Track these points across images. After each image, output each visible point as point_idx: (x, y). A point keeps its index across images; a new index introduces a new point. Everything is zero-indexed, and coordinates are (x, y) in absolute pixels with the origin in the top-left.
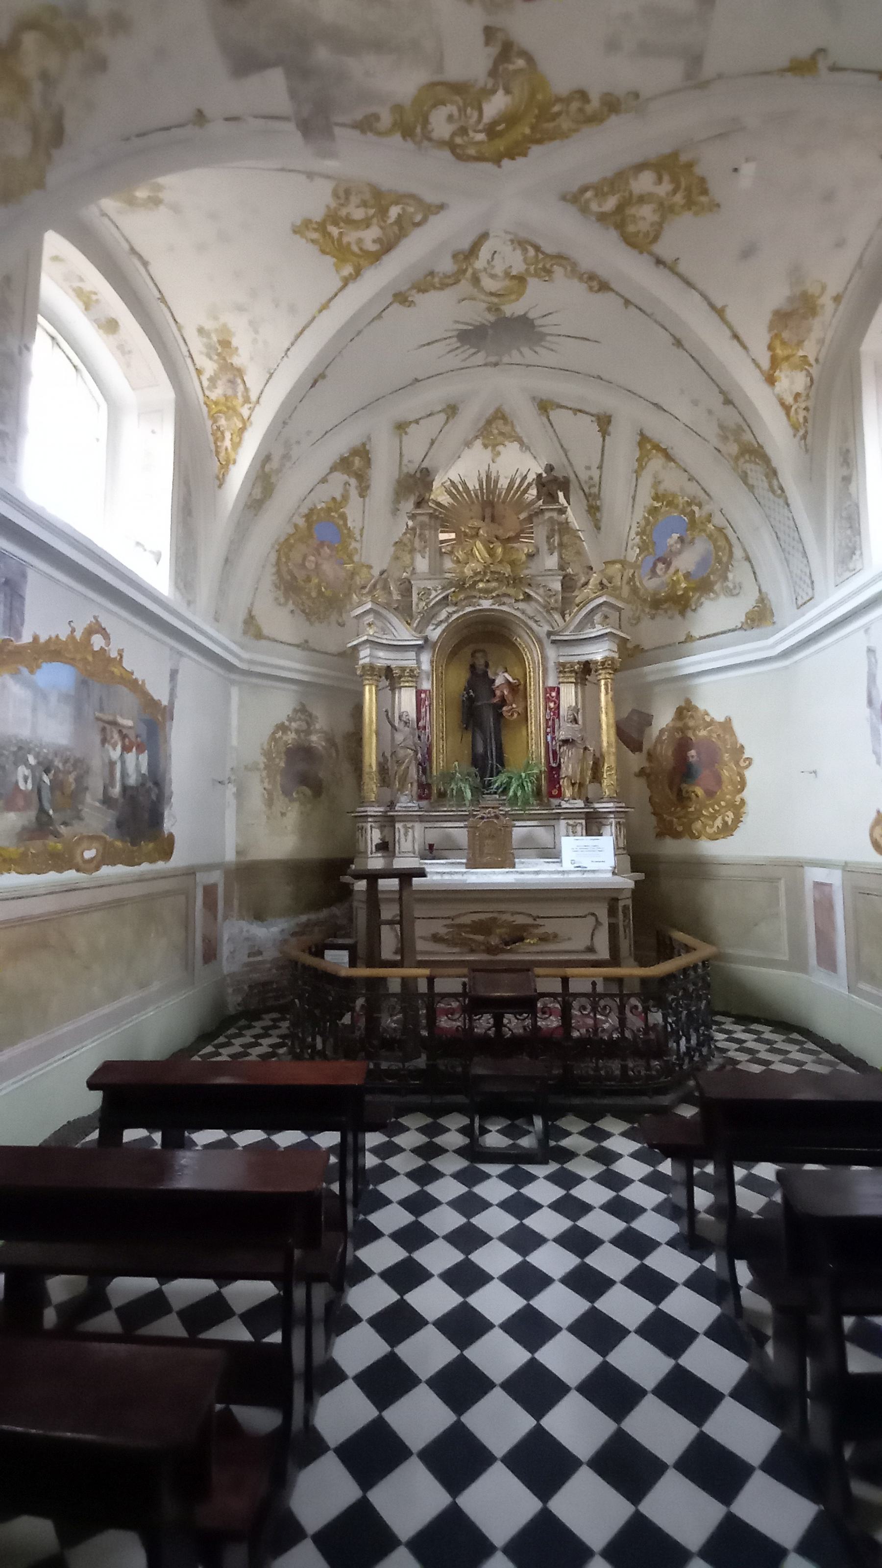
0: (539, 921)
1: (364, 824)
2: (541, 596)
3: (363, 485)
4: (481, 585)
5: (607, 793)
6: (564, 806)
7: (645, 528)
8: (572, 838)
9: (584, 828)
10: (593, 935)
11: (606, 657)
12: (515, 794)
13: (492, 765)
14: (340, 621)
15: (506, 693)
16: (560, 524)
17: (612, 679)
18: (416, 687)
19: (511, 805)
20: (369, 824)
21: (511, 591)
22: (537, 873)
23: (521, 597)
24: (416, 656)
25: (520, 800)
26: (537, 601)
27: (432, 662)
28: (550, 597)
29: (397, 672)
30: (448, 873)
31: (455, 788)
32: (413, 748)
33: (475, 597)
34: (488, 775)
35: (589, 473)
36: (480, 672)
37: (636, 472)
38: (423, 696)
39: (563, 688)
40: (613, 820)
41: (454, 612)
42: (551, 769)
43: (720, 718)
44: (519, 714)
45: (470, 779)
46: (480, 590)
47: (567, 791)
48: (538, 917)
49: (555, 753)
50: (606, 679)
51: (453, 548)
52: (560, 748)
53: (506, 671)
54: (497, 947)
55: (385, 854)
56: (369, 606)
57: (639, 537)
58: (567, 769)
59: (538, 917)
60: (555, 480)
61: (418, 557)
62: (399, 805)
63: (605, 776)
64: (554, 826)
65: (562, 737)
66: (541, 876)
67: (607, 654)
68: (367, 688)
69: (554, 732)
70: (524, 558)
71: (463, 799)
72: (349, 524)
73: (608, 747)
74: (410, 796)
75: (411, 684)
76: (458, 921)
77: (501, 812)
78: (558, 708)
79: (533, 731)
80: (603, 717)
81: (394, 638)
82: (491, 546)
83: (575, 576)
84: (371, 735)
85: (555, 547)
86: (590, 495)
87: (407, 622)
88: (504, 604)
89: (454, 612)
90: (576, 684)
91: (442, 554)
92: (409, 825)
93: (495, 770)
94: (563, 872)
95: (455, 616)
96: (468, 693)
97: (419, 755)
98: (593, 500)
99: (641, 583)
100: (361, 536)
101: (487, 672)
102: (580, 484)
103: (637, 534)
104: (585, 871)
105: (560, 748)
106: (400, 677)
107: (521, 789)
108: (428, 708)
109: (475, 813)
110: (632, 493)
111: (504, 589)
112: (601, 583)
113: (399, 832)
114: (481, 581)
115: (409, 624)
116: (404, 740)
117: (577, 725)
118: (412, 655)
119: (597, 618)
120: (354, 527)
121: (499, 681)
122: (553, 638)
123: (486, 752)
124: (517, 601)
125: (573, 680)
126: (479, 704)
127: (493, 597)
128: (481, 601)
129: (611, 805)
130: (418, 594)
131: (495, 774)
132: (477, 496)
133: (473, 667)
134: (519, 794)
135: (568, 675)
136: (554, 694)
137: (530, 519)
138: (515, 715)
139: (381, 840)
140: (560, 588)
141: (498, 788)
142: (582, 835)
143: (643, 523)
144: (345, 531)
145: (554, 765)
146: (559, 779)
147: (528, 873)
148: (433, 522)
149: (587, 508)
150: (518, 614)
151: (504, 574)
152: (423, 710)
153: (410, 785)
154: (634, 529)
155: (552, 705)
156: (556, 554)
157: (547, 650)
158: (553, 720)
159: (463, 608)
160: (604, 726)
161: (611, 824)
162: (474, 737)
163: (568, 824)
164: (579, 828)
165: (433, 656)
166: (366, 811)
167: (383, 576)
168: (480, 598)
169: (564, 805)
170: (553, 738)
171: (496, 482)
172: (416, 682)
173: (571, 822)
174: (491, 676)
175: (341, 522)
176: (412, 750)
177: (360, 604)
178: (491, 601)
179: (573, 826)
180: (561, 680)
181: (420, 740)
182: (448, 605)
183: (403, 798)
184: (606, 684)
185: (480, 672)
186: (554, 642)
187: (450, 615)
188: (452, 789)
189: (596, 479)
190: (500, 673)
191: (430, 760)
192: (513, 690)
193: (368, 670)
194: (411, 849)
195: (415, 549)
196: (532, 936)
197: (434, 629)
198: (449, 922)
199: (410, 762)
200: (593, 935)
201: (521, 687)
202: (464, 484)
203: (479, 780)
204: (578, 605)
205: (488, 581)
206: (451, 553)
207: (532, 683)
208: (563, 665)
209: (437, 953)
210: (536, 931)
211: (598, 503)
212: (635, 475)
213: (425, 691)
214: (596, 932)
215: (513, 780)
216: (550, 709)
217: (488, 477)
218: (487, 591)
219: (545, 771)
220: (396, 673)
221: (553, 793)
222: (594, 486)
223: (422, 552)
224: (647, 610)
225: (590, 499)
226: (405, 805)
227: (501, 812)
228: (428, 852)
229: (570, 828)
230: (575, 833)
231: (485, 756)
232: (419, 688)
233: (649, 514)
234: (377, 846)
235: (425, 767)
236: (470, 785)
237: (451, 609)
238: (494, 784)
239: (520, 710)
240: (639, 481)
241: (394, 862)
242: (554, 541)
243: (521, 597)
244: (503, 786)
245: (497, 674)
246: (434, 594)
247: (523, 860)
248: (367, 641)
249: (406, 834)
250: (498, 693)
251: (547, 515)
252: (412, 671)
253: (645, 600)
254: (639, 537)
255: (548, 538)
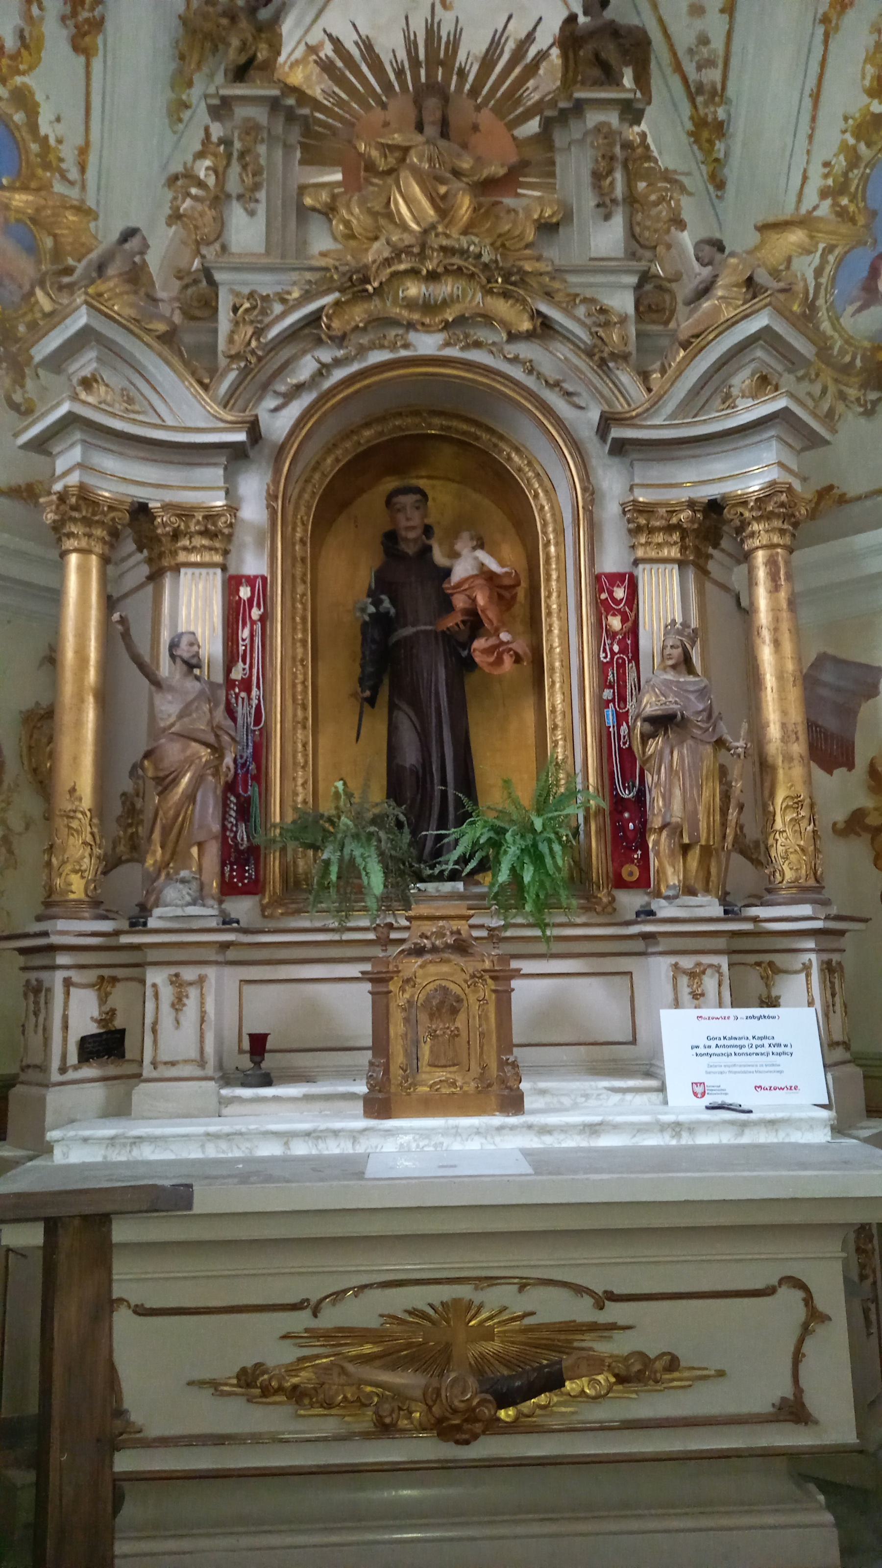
0: (615, 1312)
1: (44, 975)
2: (583, 324)
3: (84, 15)
4: (413, 289)
5: (789, 875)
6: (662, 914)
7: (845, 174)
8: (688, 1014)
9: (726, 983)
10: (797, 1357)
11: (773, 484)
12: (516, 874)
13: (444, 794)
14: (17, 397)
15: (481, 601)
16: (627, 145)
17: (784, 547)
18: (224, 568)
19: (505, 908)
20: (60, 975)
21: (502, 308)
22: (593, 1129)
23: (526, 325)
24: (227, 479)
25: (530, 897)
26: (567, 337)
27: (272, 497)
28: (607, 324)
29: (164, 521)
30: (308, 1134)
31: (335, 858)
32: (211, 739)
33: (394, 322)
34: (434, 822)
35: (699, 24)
36: (410, 550)
37: (825, 20)
38: (245, 592)
39: (646, 578)
40: (813, 957)
41: (338, 363)
42: (618, 804)
43: (836, 772)
44: (518, 659)
45: (382, 834)
46: (411, 304)
47: (670, 870)
48: (612, 1297)
49: (627, 755)
50: (771, 546)
51: (334, 197)
52: (644, 743)
53: (481, 546)
54: (471, 1415)
55: (112, 1070)
56: (81, 319)
57: (828, 202)
58: (668, 803)
59: (612, 1297)
60: (614, 31)
61: (237, 215)
62: (157, 912)
63: (779, 825)
64: (631, 973)
65: (649, 710)
66: (607, 1141)
67: (774, 474)
68: (74, 559)
69: (622, 699)
70: (530, 235)
71: (360, 891)
72: (45, 128)
73: (785, 739)
74: (195, 885)
75: (207, 557)
76: (330, 1318)
77: (476, 933)
78: (634, 631)
79: (559, 707)
80: (766, 655)
81: (159, 422)
82: (443, 190)
83: (670, 281)
84: (81, 700)
85: (614, 201)
86: (700, 88)
87: (201, 383)
88: (478, 345)
89: (338, 363)
90: (682, 564)
91: (303, 213)
92: (189, 974)
93: (451, 809)
94: (677, 1128)
95: (339, 374)
96: (377, 603)
97: (228, 760)
98: (706, 104)
99: (835, 321)
100: (83, 169)
101: (428, 549)
102: (674, 54)
103: (824, 194)
104: (744, 1125)
105: (644, 743)
106: (176, 535)
107: (534, 863)
108: (258, 627)
109: (394, 935)
110: (811, 83)
111: (477, 299)
112: (750, 282)
113: (156, 996)
114: (413, 273)
115: (205, 387)
116: (180, 716)
117: (691, 678)
118: (215, 475)
119: (742, 379)
120: (60, 141)
121: (462, 570)
122: (616, 433)
123: (426, 762)
124: (513, 337)
125: (674, 552)
126: (409, 631)
127: (447, 326)
128: (412, 336)
129: (806, 910)
130: (235, 309)
131: (451, 817)
132: (400, 73)
133: (391, 538)
134: (527, 876)
135: (659, 538)
136: (620, 593)
137: (545, 138)
138: (508, 660)
139: (100, 1022)
140: (630, 309)
141: (464, 860)
142: (721, 1005)
143: (841, 163)
144: (34, 147)
145: (626, 795)
146: (642, 831)
147: (565, 1129)
148: (279, 128)
149: (689, 126)
150: (517, 373)
151: (479, 256)
152: (245, 633)
153: (195, 851)
154: (816, 182)
155: (615, 623)
156: (618, 222)
157: (600, 472)
158: (621, 666)
159: (362, 351)
160: (770, 680)
161: (807, 968)
162: (392, 730)
163: (676, 966)
164: (710, 983)
165: (276, 481)
166: (45, 934)
167: (127, 246)
168: (411, 326)
169: (664, 909)
170: (621, 718)
171: (454, 44)
172: (226, 553)
173: (687, 962)
174: (439, 557)
175: (19, 117)
176: (207, 745)
177: (55, 318)
178: (439, 338)
179: (694, 975)
180: (640, 553)
181: (234, 719)
182: (319, 342)
183: (171, 893)
184: (772, 563)
185: (410, 550)
186: (620, 448)
187: (324, 370)
188: (327, 863)
189: (718, 44)
190: (465, 552)
191: (260, 777)
192: (500, 597)
193: (75, 508)
194: (194, 1054)
195: (229, 196)
196: (597, 1364)
197: (276, 410)
198: (301, 1321)
199: (198, 781)
200: (797, 1357)
201: (521, 593)
202: (367, 46)
203: (407, 837)
204: (685, 345)
205: (433, 277)
206: (329, 211)
207: (554, 575)
208: (646, 510)
209: (256, 1439)
210: (603, 1348)
211: (721, 114)
212: (820, 30)
213: (251, 581)
214: (808, 1347)
215: (508, 836)
216: (612, 635)
217: (432, 32)
218: (428, 307)
219: (599, 811)
220: (164, 525)
221: (625, 875)
222: (709, 63)
223: (247, 197)
224: (852, 393)
225: (700, 99)
226: (179, 912)
227: (476, 933)
228: (245, 1062)
229: (684, 980)
230: (697, 996)
231: (423, 777)
232: (232, 571)
233: (858, 137)
234: (84, 1041)
235: (248, 800)
236: (381, 854)
237: (326, 355)
238: (449, 851)
239: (521, 646)
240: (832, 46)
241: (135, 1098)
242: (612, 183)
243: (526, 325)
244: (478, 856)
245: (455, 555)
246: (278, 308)
247: (542, 1085)
248: (71, 421)
249: (178, 1004)
250: (460, 602)
251: (593, 118)
252: (211, 517)
253: (846, 369)
254: (828, 202)
255: (598, 177)
